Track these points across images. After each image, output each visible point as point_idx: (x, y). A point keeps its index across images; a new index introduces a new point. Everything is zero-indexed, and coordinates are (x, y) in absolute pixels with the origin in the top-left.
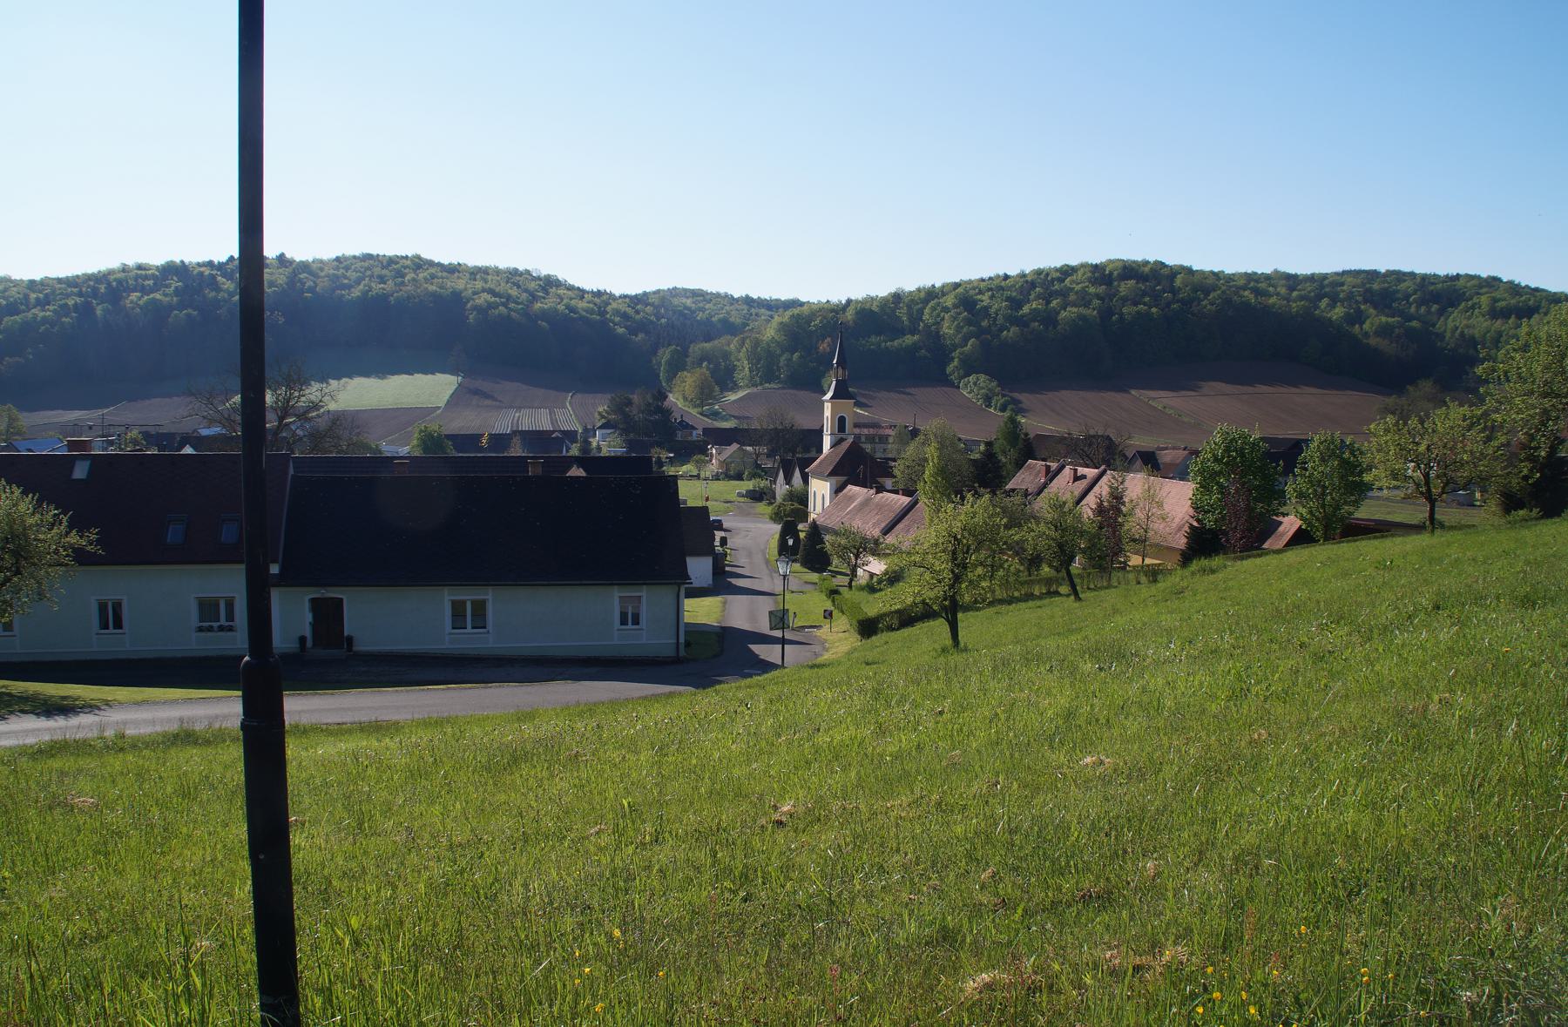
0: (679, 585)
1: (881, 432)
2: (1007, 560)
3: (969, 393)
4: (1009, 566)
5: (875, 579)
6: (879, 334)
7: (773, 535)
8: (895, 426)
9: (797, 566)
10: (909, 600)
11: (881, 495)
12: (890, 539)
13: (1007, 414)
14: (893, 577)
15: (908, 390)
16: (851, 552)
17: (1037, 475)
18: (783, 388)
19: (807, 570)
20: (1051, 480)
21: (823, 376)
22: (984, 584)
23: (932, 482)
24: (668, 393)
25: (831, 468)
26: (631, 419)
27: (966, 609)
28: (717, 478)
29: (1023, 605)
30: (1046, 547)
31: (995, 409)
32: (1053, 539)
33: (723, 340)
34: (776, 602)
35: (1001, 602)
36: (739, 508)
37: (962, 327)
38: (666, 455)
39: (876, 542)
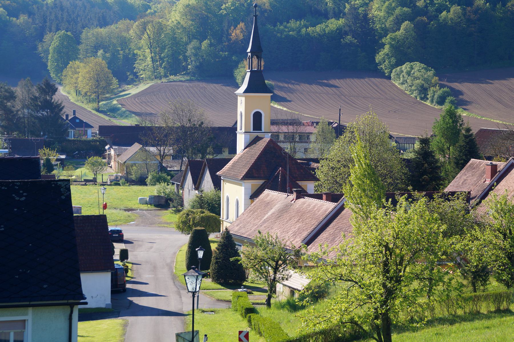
0: (72, 306)
1: (302, 129)
2: (447, 273)
3: (403, 84)
4: (450, 280)
5: (297, 295)
6: (298, 17)
7: (181, 246)
8: (317, 123)
9: (208, 282)
10: (336, 319)
11: (302, 200)
12: (314, 249)
13: (446, 106)
14: (317, 293)
15: (332, 82)
16: (270, 265)
17: (481, 176)
18: (190, 81)
19: (219, 286)
20: (498, 181)
21: (236, 66)
22: (422, 300)
23: (359, 185)
24: (57, 86)
25: (246, 170)
26: (14, 115)
27: (402, 329)
28: (116, 182)
29: (467, 325)
30: (493, 258)
31: (432, 102)
32: (501, 248)
33: (121, 24)
34: (185, 323)
35: (442, 321)
36: (141, 216)
37: (394, 9)
38: (54, 157)
39: (298, 253)
